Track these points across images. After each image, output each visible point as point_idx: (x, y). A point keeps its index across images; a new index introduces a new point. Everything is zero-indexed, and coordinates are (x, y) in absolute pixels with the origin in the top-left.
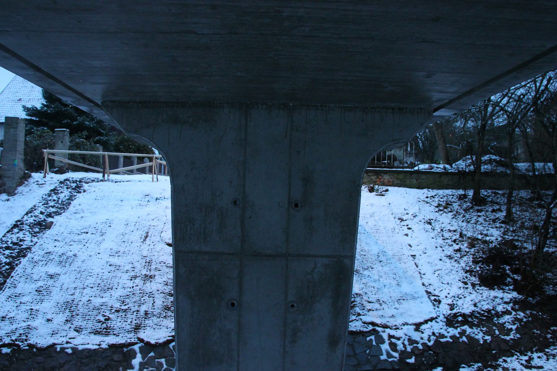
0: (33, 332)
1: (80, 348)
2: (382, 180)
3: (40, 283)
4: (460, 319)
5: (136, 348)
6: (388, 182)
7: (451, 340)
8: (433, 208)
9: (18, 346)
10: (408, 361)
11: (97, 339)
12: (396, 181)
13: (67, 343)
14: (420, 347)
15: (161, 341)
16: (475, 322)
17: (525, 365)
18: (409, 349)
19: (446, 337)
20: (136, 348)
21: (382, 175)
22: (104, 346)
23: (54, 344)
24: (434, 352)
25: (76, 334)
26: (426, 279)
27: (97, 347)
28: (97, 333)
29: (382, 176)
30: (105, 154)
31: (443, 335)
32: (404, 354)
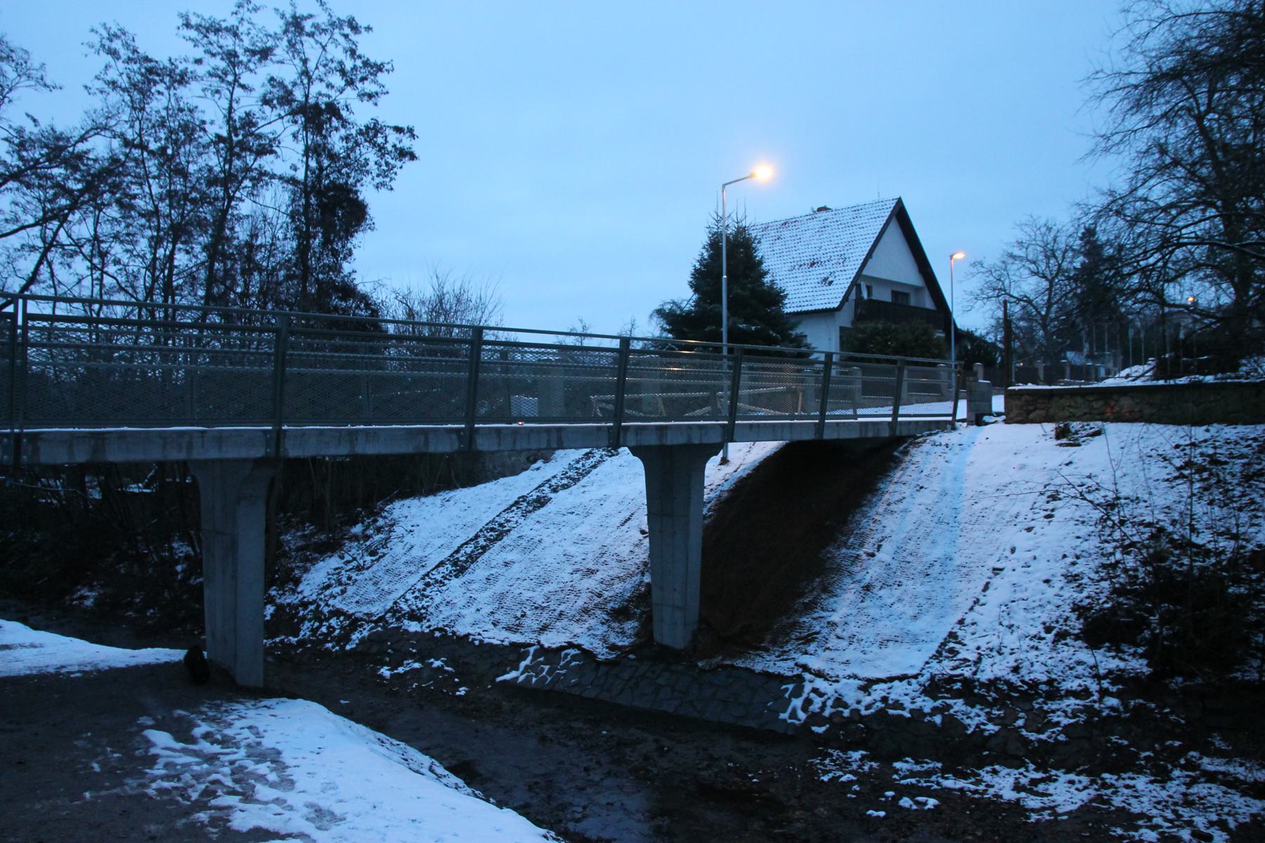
0: (461, 620)
1: (486, 641)
2: (1117, 409)
3: (493, 571)
4: (958, 686)
5: (532, 650)
6: (1131, 412)
7: (909, 715)
8: (1170, 469)
9: (446, 631)
10: (814, 728)
11: (505, 634)
12: (1147, 411)
13: (479, 634)
14: (846, 713)
15: (554, 646)
16: (990, 698)
17: (1181, 802)
18: (827, 713)
19: (904, 709)
20: (532, 650)
21: (1116, 397)
22: (506, 643)
23: (469, 634)
24: (866, 726)
25: (492, 627)
26: (22, 646)
27: (499, 642)
28: (508, 629)
29: (1117, 401)
30: (655, 398)
31: (902, 704)
32: (816, 718)
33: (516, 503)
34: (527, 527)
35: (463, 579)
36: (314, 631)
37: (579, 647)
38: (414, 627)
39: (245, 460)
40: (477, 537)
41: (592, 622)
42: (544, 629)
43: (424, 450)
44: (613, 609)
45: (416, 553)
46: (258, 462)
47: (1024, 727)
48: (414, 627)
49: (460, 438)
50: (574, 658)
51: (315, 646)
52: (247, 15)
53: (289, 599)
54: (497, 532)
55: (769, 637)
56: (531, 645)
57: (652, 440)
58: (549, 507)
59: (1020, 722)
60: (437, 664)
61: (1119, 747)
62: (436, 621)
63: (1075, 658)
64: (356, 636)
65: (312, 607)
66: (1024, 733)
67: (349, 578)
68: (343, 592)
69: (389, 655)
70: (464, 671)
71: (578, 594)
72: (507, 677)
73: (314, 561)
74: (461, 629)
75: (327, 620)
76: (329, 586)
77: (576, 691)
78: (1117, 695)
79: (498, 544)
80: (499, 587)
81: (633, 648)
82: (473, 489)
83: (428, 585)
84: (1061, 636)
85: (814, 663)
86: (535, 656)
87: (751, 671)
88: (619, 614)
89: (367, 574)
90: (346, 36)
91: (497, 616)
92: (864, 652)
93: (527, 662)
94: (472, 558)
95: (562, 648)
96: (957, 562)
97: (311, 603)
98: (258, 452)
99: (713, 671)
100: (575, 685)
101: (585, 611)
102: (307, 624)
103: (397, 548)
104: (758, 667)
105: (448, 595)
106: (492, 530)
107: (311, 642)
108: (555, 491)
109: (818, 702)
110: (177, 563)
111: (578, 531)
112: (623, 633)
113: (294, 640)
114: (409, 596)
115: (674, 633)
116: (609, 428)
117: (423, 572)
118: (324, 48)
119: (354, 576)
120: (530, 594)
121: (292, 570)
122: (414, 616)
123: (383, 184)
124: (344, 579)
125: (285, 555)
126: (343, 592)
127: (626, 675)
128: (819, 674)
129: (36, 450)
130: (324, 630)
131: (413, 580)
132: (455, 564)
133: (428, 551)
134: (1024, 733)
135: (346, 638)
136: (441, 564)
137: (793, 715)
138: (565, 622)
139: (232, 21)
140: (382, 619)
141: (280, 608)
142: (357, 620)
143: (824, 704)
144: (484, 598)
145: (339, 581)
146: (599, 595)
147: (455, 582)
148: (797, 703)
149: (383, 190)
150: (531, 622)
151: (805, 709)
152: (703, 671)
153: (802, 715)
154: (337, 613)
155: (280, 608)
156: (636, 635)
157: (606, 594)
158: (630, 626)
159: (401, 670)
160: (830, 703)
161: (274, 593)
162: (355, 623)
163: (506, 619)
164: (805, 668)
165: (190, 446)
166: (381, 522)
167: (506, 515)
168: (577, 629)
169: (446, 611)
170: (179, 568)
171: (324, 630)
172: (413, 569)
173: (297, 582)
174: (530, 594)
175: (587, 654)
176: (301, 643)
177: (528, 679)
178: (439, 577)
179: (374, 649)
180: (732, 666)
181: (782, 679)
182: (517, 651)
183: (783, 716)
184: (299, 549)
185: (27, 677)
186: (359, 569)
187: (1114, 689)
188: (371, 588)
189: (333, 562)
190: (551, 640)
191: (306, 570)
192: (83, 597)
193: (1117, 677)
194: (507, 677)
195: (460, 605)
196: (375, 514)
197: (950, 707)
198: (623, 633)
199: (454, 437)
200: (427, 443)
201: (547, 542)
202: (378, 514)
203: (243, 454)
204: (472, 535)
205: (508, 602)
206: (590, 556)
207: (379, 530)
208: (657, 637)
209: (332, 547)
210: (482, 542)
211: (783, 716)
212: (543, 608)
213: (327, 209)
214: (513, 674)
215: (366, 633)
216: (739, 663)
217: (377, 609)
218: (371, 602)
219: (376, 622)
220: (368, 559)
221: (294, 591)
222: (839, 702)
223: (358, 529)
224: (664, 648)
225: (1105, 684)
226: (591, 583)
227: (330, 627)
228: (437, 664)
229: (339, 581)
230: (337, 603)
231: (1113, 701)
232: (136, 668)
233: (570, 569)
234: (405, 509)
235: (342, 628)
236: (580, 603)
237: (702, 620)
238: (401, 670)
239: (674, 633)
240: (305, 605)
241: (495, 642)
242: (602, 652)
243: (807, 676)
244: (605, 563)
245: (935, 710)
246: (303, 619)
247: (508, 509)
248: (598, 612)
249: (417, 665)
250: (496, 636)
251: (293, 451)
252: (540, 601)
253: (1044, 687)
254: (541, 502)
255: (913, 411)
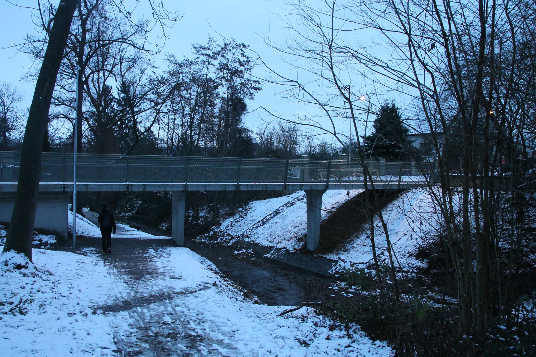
5: (274, 248)
18: (340, 271)
20: (274, 248)
28: (270, 242)
32: (337, 272)
33: (286, 204)
34: (285, 212)
35: (263, 226)
36: (221, 240)
37: (286, 248)
38: (246, 240)
39: (179, 191)
40: (272, 214)
41: (292, 241)
42: (279, 242)
43: (225, 190)
44: (299, 238)
45: (254, 218)
46: (182, 192)
47: (388, 280)
48: (246, 240)
49: (235, 187)
50: (284, 251)
51: (220, 245)
52: (211, 44)
53: (217, 230)
54: (277, 213)
55: (336, 249)
56: (274, 247)
57: (309, 188)
58: (295, 206)
59: (388, 278)
60: (250, 251)
61: (410, 287)
62: (252, 239)
63: (410, 262)
64: (231, 242)
65: (222, 233)
66: (388, 281)
67: (234, 224)
68: (231, 228)
69: (239, 248)
70: (256, 254)
71: (290, 232)
72: (266, 256)
73: (226, 219)
74: (258, 242)
75: (226, 237)
76: (228, 227)
77: (281, 261)
78: (416, 273)
79: (276, 217)
80: (271, 230)
81: (300, 250)
82: (277, 199)
83: (254, 228)
84: (411, 255)
85: (342, 257)
86: (275, 250)
87: (326, 258)
88: (300, 240)
89: (239, 223)
90: (241, 49)
91: (268, 238)
92: (357, 255)
93: (272, 252)
94: (268, 220)
95: (282, 248)
96: (396, 231)
97: (222, 231)
98: (181, 189)
99: (317, 257)
100: (282, 259)
101: (291, 238)
102: (220, 238)
103: (249, 216)
104: (328, 257)
105: (258, 231)
106: (276, 212)
107: (220, 243)
108: (298, 200)
109: (339, 268)
110: (190, 217)
111: (299, 214)
112: (299, 245)
113: (216, 242)
114: (248, 231)
115: (311, 247)
116: (283, 184)
117: (254, 224)
118: (234, 54)
119: (235, 224)
120: (279, 232)
121: (220, 221)
122: (248, 237)
123: (251, 98)
124: (233, 225)
125: (219, 216)
126: (231, 228)
127: (295, 257)
128: (343, 261)
129: (132, 188)
130: (224, 239)
131: (250, 226)
132: (263, 222)
133: (257, 217)
134: (388, 281)
135: (229, 242)
136: (259, 221)
137: (332, 271)
138: (285, 241)
139: (207, 46)
140: (239, 237)
141: (214, 232)
142: (233, 237)
143: (340, 269)
144: (267, 232)
145: (231, 225)
146: (297, 234)
147: (261, 227)
148: (334, 268)
149: (251, 100)
150: (276, 241)
151: (335, 270)
152: (315, 257)
153: (334, 271)
154: (228, 235)
155: (214, 232)
156: (302, 246)
157: (298, 233)
158: (302, 243)
159: (240, 252)
160: (342, 269)
161: (213, 228)
162: (232, 238)
163: (270, 239)
164: (340, 258)
165: (165, 187)
166: (247, 207)
167: (282, 208)
168: (288, 243)
169: (256, 236)
170: (190, 219)
171: (224, 239)
172: (251, 223)
173: (220, 225)
174: (279, 232)
175: (288, 250)
176: (218, 243)
177: (271, 256)
178: (257, 226)
179: (235, 246)
180: (322, 257)
181: (333, 261)
182: (271, 248)
183: (330, 271)
184: (223, 215)
185: (132, 239)
186: (237, 222)
187: (416, 271)
188: (239, 228)
189: (231, 219)
190: (280, 246)
191: (223, 221)
192: (163, 226)
193: (418, 268)
194: (266, 256)
195: (260, 234)
196: (247, 204)
197: (371, 272)
198: (299, 245)
199: (234, 186)
200: (226, 188)
201: (289, 216)
202: (247, 205)
203: (177, 190)
204: (270, 214)
205: (272, 234)
206: (298, 222)
207: (246, 210)
208: (307, 247)
209: (232, 214)
210: (272, 215)
211: (330, 271)
212: (281, 237)
213: (234, 106)
214: (268, 255)
215: (234, 241)
216: (325, 256)
217: (238, 234)
218: (238, 232)
219: (237, 238)
220: (241, 219)
221: (219, 227)
222: (344, 268)
223: (240, 209)
224: (308, 250)
225: (414, 270)
226: (296, 230)
227: (226, 239)
228: (250, 251)
229: (231, 225)
230: (229, 232)
231: (414, 275)
232: (156, 239)
233: (292, 225)
234: (256, 204)
235: (229, 239)
236: (291, 236)
237: (320, 243)
238: (240, 252)
239: (311, 247)
240: (221, 232)
241: (266, 245)
242: (291, 250)
243: (339, 261)
244: (301, 224)
245: (368, 273)
246: (219, 236)
247: (283, 206)
248: (295, 239)
249: (245, 251)
250: (266, 244)
251: (190, 189)
252: (280, 234)
253: (398, 269)
254: (293, 204)
255: (406, 179)
